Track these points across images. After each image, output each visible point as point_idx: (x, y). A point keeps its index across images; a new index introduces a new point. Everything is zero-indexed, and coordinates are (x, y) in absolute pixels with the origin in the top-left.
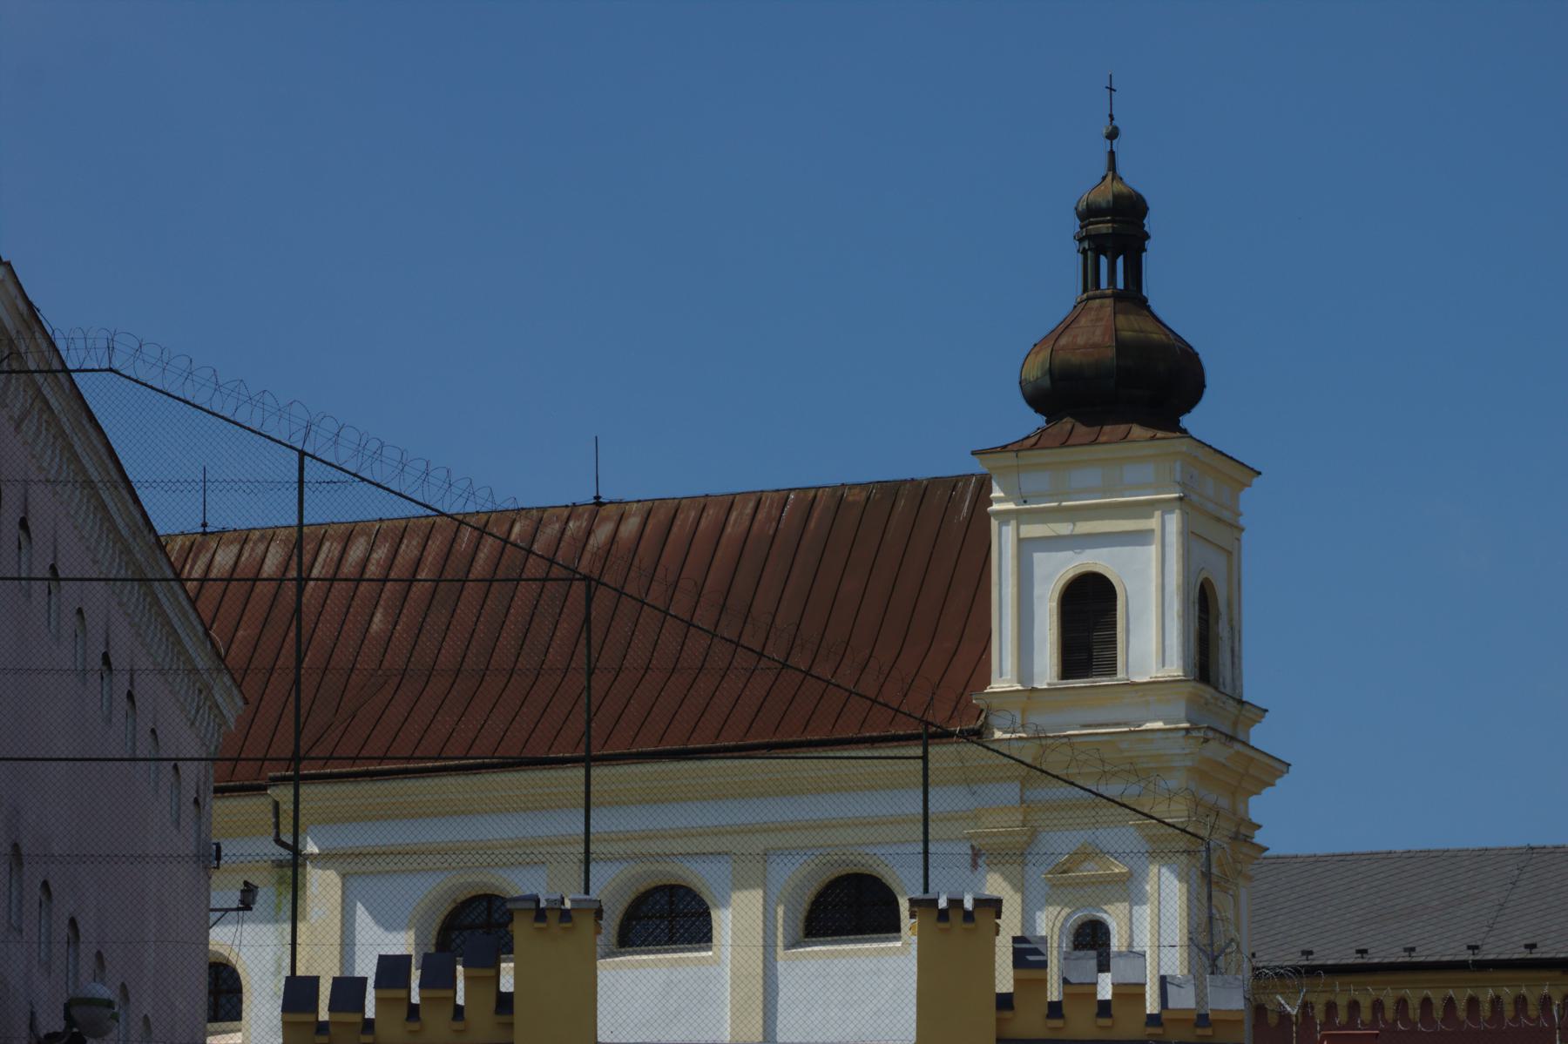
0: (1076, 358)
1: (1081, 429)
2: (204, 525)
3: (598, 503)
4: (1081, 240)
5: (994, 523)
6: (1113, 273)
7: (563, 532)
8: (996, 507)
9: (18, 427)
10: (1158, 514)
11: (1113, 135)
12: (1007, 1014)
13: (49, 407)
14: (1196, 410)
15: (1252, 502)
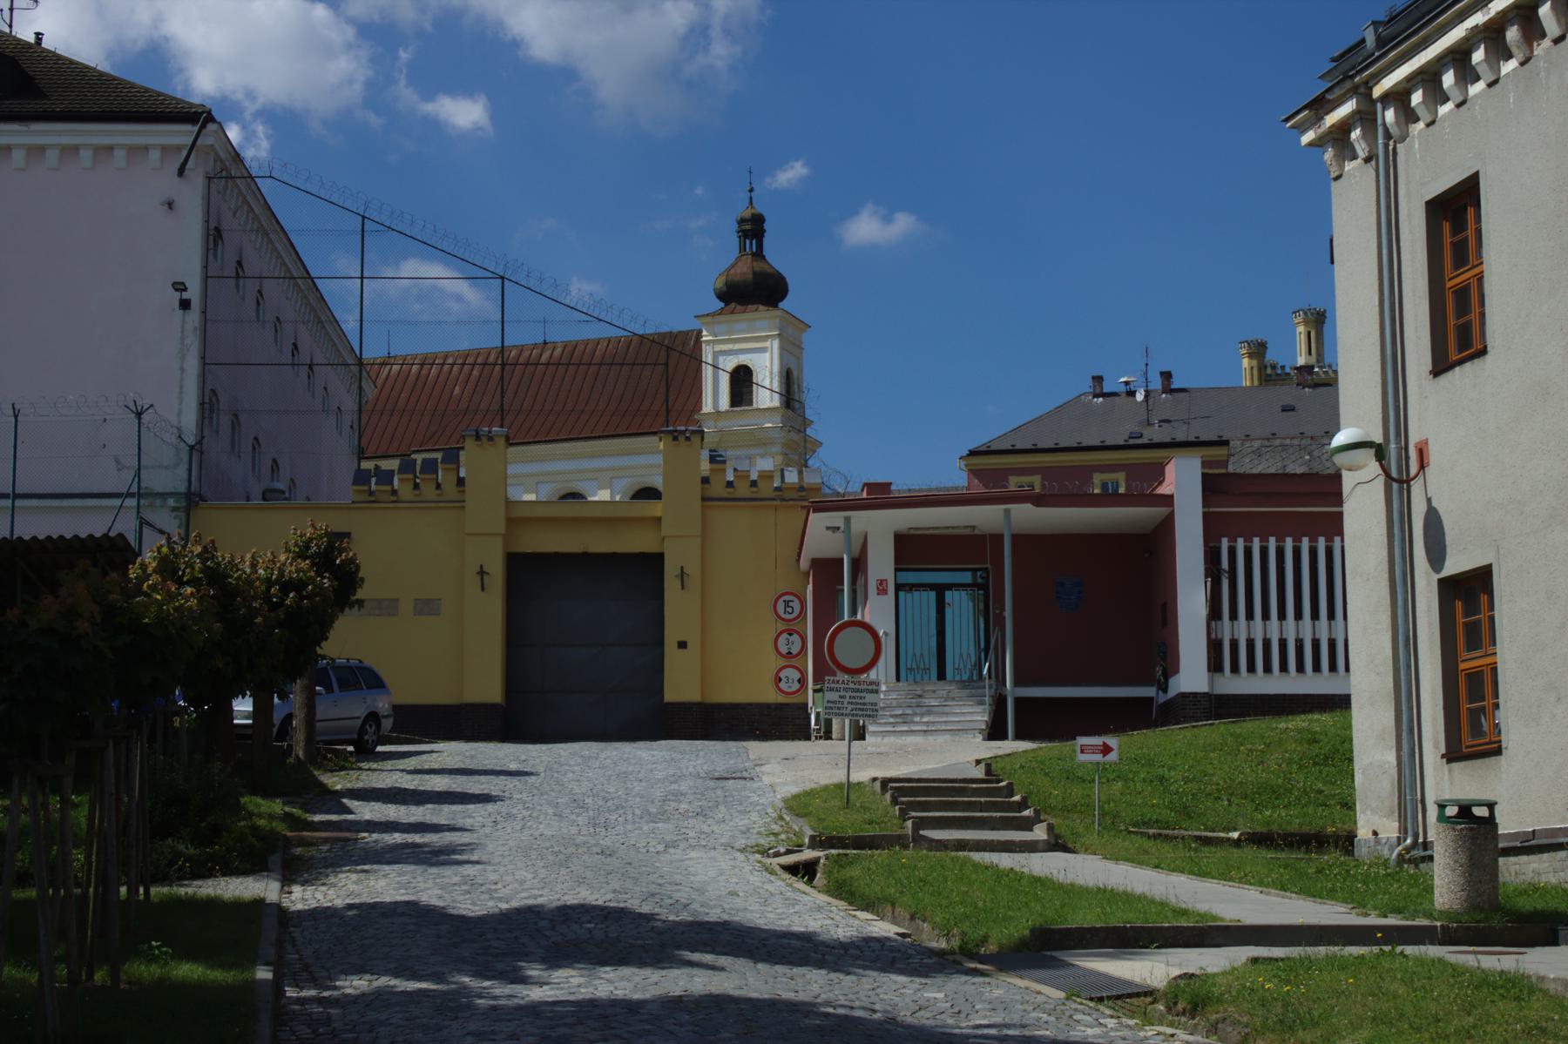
0: (737, 278)
1: (739, 307)
2: (389, 354)
3: (545, 343)
4: (738, 232)
5: (704, 345)
6: (751, 245)
7: (531, 354)
8: (704, 339)
9: (234, 214)
10: (770, 340)
11: (751, 190)
12: (707, 486)
13: (252, 210)
14: (785, 301)
15: (807, 338)
